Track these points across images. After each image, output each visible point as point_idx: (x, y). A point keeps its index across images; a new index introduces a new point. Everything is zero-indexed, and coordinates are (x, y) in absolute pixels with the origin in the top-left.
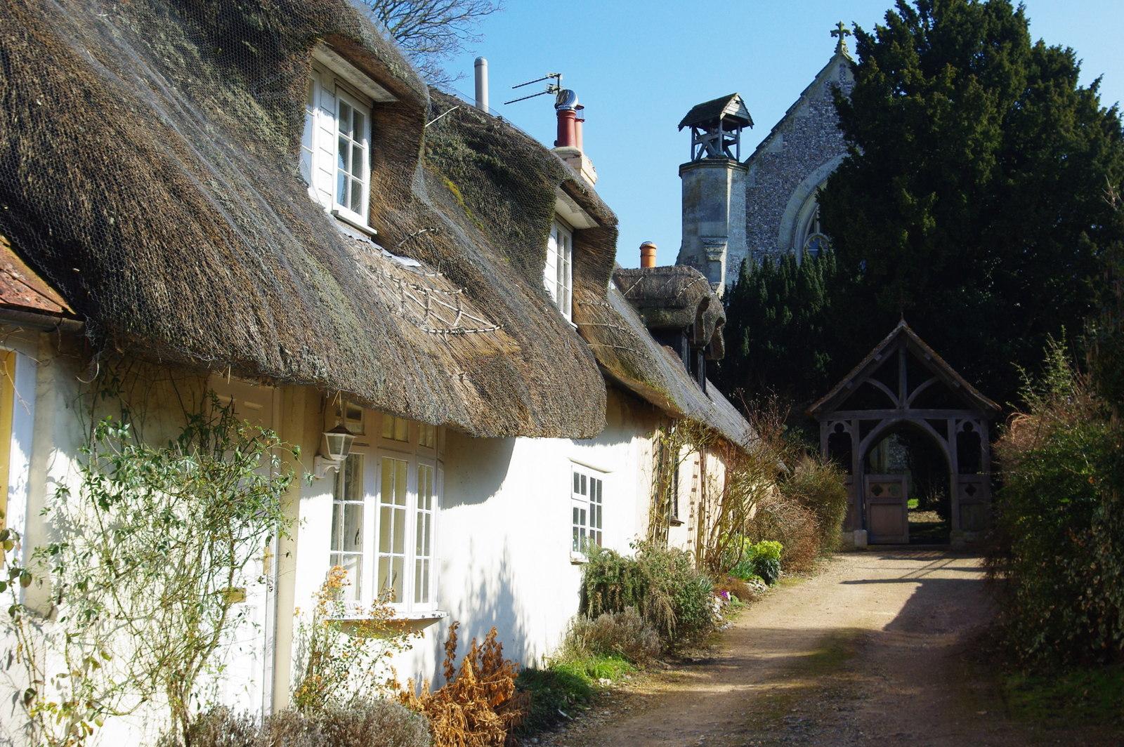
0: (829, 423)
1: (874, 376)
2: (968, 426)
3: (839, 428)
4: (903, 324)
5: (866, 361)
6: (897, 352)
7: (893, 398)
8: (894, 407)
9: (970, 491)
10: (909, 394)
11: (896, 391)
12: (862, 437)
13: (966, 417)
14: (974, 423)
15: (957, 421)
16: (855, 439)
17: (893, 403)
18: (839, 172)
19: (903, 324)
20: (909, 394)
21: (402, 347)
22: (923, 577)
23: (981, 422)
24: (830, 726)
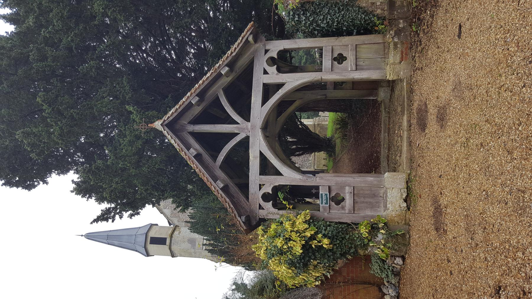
0: (260, 207)
1: (214, 158)
2: (272, 61)
3: (266, 197)
4: (158, 125)
5: (195, 165)
6: (195, 135)
7: (238, 139)
8: (247, 138)
9: (340, 59)
10: (235, 123)
11: (232, 135)
12: (278, 173)
13: (261, 64)
14: (269, 55)
15: (265, 72)
16: (278, 181)
17: (243, 139)
18: (145, 205)
19: (158, 125)
20: (235, 123)
21: (456, 97)
22: (369, 286)
23: (267, 48)
24: (234, 245)
